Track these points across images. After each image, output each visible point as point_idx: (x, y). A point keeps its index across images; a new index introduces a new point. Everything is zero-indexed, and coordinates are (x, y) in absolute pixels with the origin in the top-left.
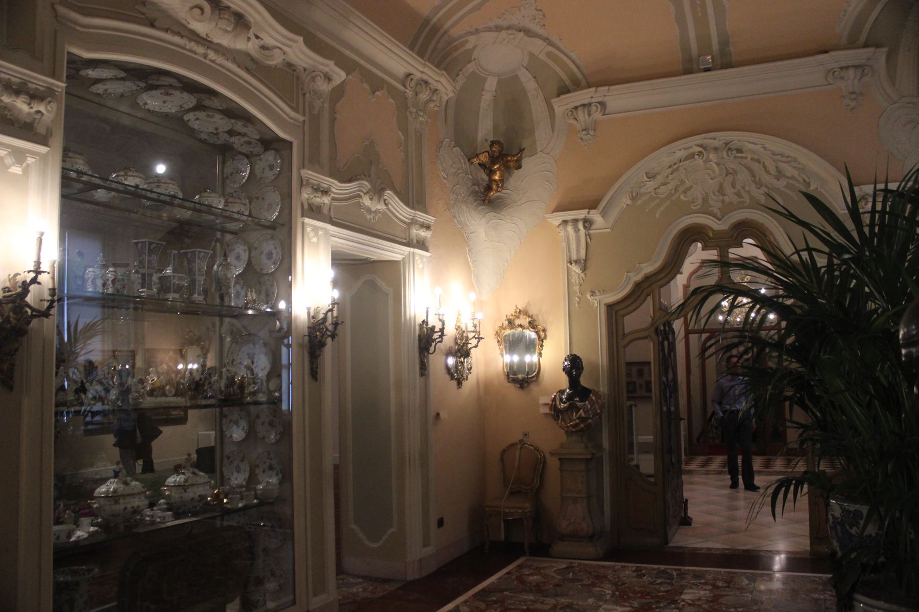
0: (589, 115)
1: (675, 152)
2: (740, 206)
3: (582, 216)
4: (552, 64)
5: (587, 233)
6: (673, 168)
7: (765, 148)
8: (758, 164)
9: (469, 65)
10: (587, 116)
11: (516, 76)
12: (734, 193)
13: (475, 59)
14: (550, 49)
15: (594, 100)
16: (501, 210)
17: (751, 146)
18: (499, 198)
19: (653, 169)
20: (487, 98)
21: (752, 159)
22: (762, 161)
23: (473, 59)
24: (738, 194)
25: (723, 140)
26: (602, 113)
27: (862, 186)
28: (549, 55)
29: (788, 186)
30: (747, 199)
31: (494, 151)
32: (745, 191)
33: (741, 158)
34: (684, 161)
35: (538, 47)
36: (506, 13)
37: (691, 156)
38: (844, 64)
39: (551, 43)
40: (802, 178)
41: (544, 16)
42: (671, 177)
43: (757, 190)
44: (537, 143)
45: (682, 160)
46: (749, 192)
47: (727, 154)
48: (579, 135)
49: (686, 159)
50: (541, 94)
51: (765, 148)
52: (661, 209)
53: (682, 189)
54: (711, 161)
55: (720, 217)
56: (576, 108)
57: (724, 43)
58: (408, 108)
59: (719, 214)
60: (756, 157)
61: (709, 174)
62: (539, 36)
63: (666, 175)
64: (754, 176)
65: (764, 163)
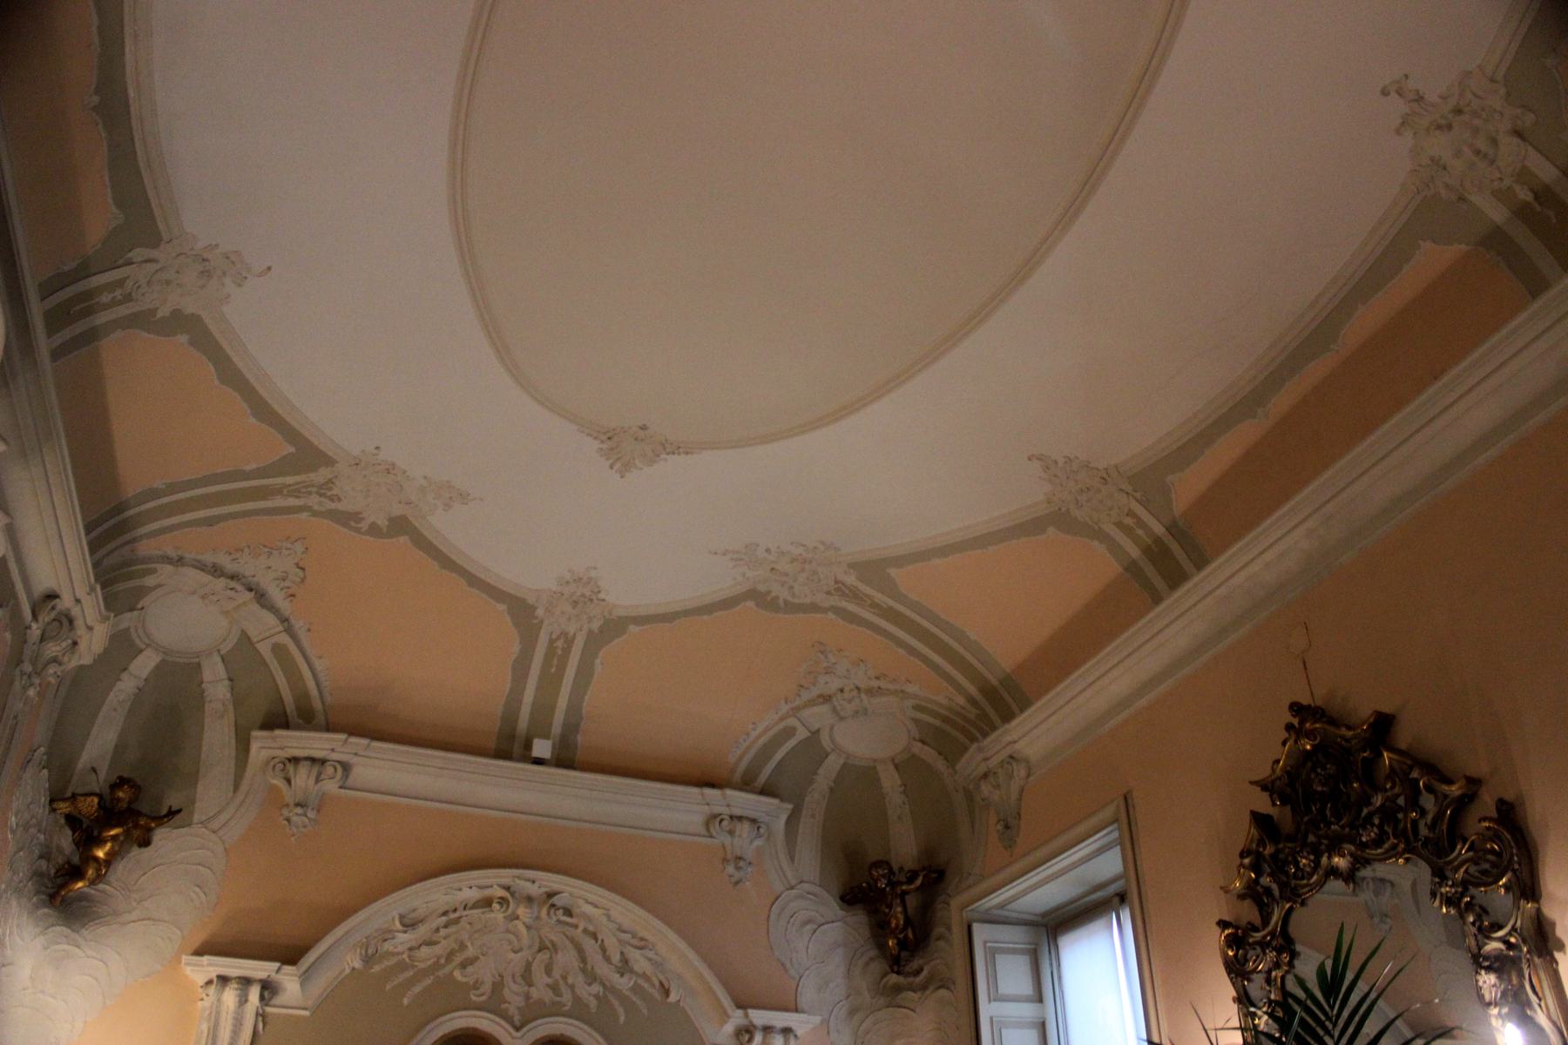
0: (317, 780)
1: (460, 890)
2: (554, 1010)
3: (262, 975)
4: (274, 666)
5: (261, 1011)
6: (451, 916)
7: (609, 917)
8: (593, 942)
9: (128, 615)
10: (312, 781)
11: (199, 665)
12: (548, 985)
13: (142, 608)
14: (285, 639)
15: (335, 756)
16: (83, 926)
17: (588, 909)
18: (83, 897)
19: (414, 910)
20: (126, 686)
21: (585, 931)
22: (600, 938)
23: (139, 606)
24: (554, 988)
25: (546, 886)
26: (340, 784)
27: (750, 1011)
28: (278, 649)
29: (636, 989)
30: (567, 998)
31: (119, 799)
32: (566, 983)
33: (567, 924)
34: (472, 908)
35: (261, 625)
36: (246, 550)
37: (487, 903)
38: (738, 812)
39: (290, 631)
40: (658, 979)
41: (303, 580)
42: (443, 932)
43: (586, 987)
44: (198, 804)
45: (469, 906)
46: (572, 987)
47: (548, 914)
48: (285, 812)
49: (475, 906)
50: (232, 715)
51: (609, 917)
52: (417, 989)
53: (458, 959)
54: (517, 918)
55: (518, 1024)
56: (295, 760)
57: (572, 727)
58: (22, 662)
59: (517, 1018)
60: (591, 928)
61: (510, 942)
62: (272, 609)
63: (434, 925)
64: (583, 960)
65: (603, 941)
